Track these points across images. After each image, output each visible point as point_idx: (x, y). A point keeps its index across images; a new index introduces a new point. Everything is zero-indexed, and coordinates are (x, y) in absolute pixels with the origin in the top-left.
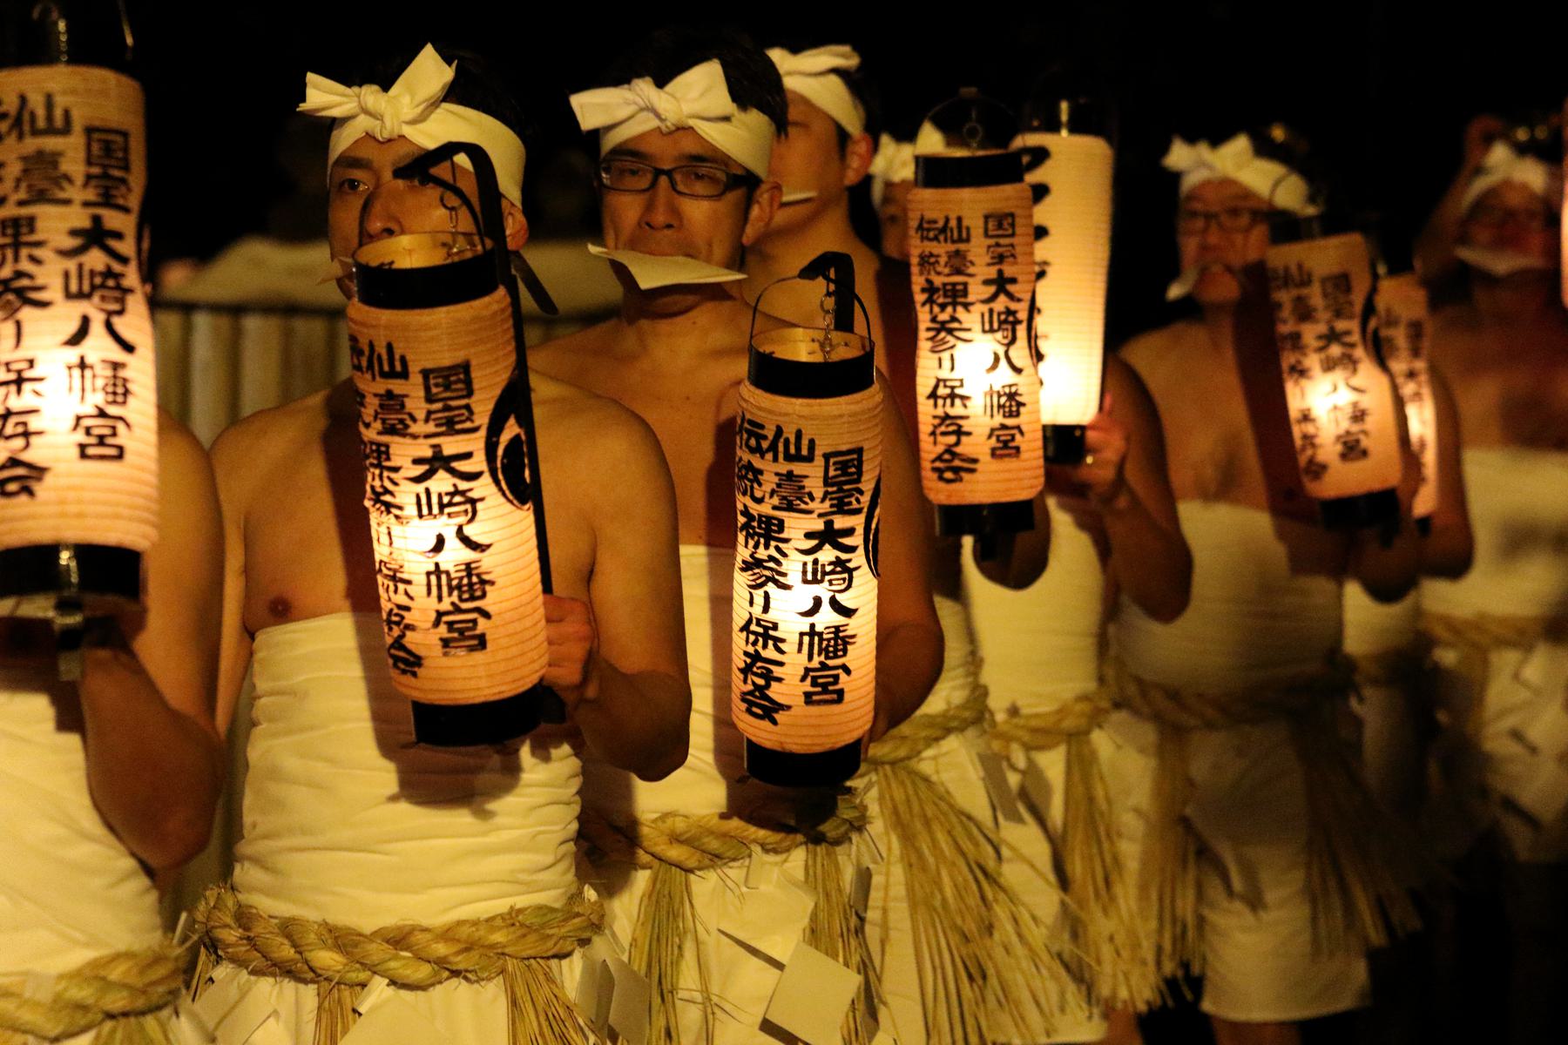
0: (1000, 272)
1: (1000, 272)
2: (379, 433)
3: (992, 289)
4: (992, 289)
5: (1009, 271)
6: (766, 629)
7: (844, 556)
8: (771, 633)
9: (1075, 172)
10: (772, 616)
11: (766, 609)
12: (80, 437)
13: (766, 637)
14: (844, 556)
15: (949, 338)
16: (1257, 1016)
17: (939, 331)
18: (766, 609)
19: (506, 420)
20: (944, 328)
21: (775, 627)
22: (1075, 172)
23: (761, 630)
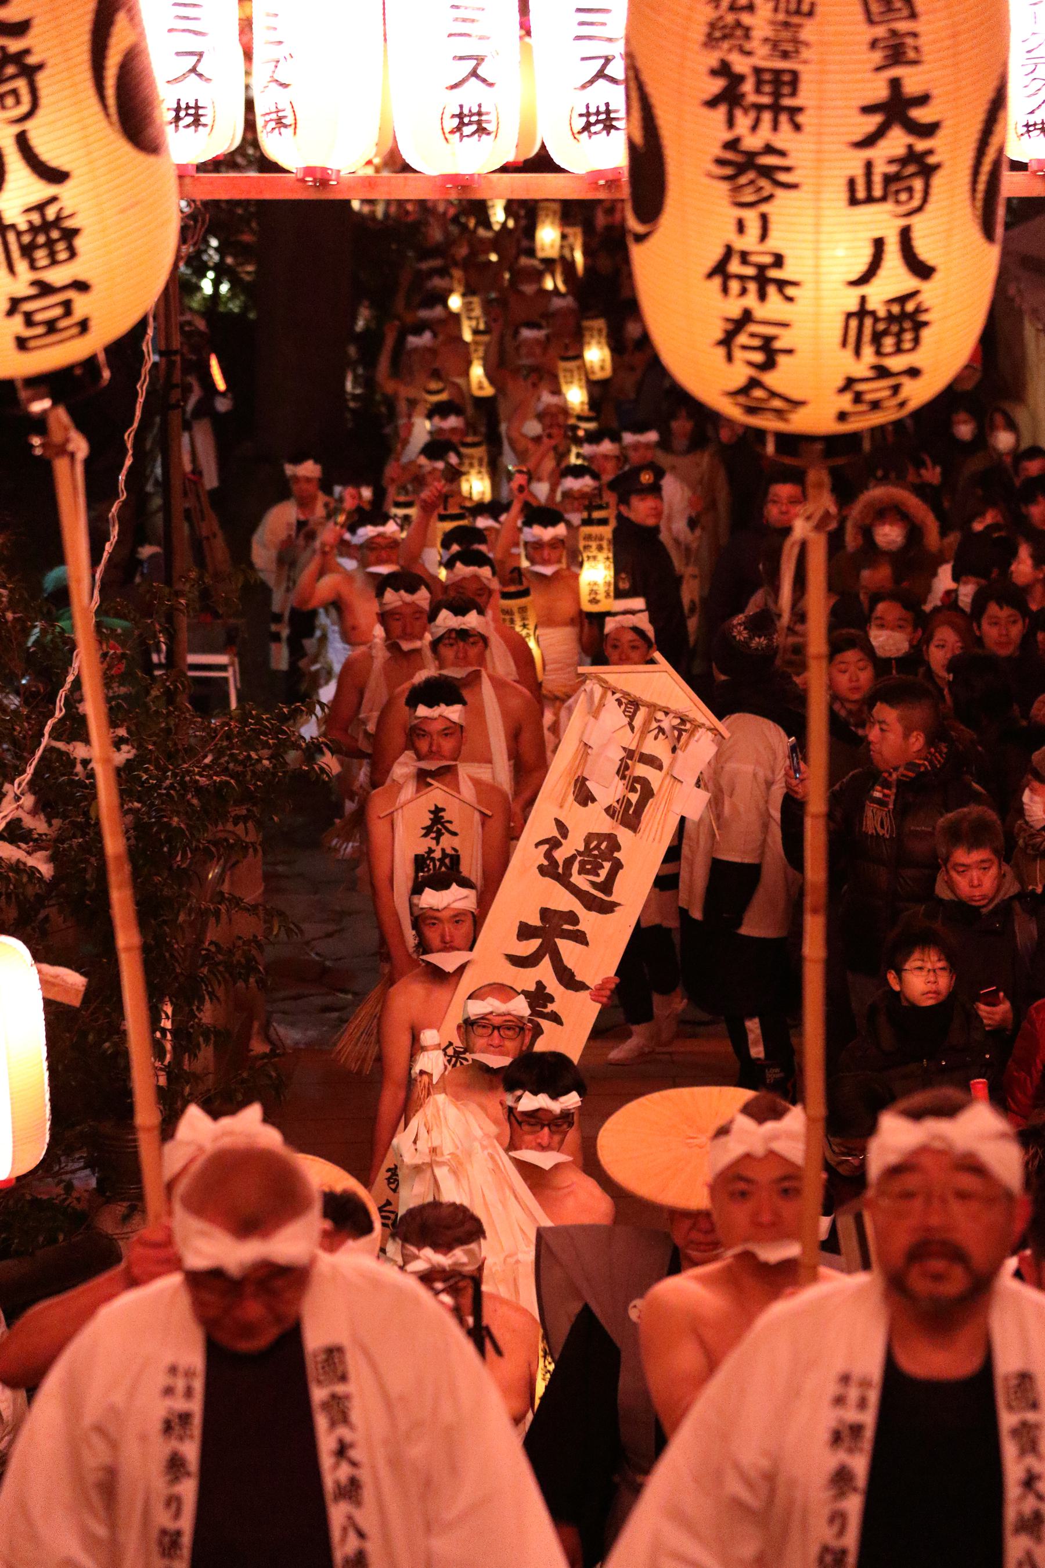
0: (895, 84)
1: (895, 84)
2: (87, 741)
3: (874, 121)
4: (874, 121)
5: (913, 82)
6: (762, 268)
7: (921, 145)
8: (773, 273)
9: (570, 1159)
10: (776, 242)
11: (764, 236)
12: (16, 325)
13: (762, 281)
14: (921, 145)
15: (763, 183)
16: (736, 859)
17: (741, 169)
18: (764, 236)
19: (163, 479)
20: (603, 361)
21: (779, 261)
22: (570, 1159)
23: (750, 271)
